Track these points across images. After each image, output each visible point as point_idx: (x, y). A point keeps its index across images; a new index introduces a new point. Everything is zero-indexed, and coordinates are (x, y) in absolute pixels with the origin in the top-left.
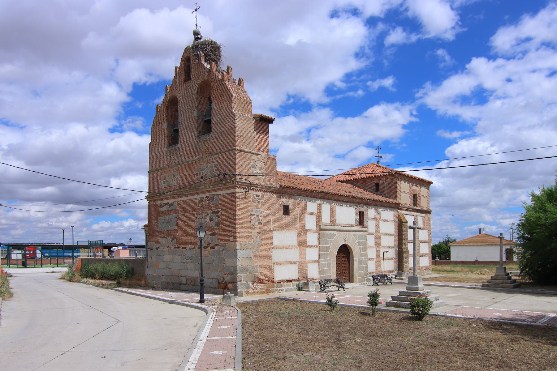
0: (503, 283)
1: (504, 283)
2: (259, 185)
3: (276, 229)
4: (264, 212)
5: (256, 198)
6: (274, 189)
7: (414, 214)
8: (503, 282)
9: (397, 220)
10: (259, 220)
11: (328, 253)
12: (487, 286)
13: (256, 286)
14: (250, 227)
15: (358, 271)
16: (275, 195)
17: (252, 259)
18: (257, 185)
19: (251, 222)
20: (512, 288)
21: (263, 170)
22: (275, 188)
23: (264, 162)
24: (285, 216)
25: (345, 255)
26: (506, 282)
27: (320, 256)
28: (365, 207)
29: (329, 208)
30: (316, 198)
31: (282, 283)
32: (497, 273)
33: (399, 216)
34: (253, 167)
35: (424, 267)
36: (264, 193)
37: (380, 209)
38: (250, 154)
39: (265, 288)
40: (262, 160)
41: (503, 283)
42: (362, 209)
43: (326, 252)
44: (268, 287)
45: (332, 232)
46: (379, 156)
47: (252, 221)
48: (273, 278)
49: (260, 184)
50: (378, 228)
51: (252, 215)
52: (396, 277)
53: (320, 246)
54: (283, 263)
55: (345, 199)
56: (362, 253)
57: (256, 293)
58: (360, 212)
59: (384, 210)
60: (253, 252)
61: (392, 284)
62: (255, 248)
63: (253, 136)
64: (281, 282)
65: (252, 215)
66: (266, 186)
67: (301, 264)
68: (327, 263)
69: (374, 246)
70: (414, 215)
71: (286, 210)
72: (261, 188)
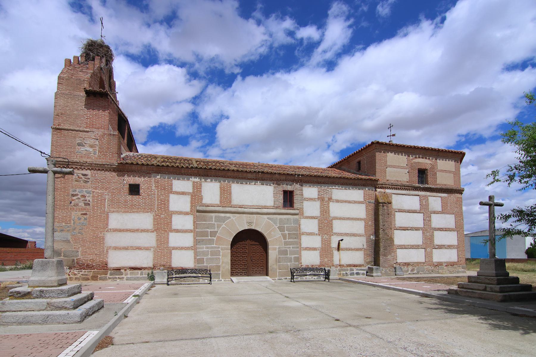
0: (485, 290)
1: (488, 289)
2: (85, 164)
3: (115, 210)
4: (94, 192)
5: (83, 177)
6: (109, 166)
7: (419, 194)
8: (486, 287)
9: (373, 201)
10: (86, 200)
11: (214, 239)
12: (454, 293)
13: (76, 272)
14: (69, 208)
15: (279, 262)
16: (114, 174)
17: (70, 242)
18: (81, 163)
19: (71, 203)
20: (498, 301)
21: (96, 147)
22: (112, 165)
23: (97, 139)
24: (131, 196)
25: (257, 243)
26: (491, 288)
27: (197, 242)
28: (298, 186)
29: (219, 186)
30: (191, 175)
31: (122, 271)
32: (481, 271)
33: (375, 196)
34: (79, 145)
35: (445, 262)
36: (95, 172)
37: (330, 187)
38: (74, 132)
39: (91, 274)
40: (94, 137)
41: (485, 290)
42: (289, 188)
43: (210, 238)
44: (95, 274)
45: (223, 215)
46: (391, 135)
47: (73, 202)
48: (106, 265)
49: (86, 162)
50: (325, 211)
51: (73, 195)
52: (367, 273)
53: (197, 230)
54: (126, 248)
55: (249, 176)
56: (287, 240)
57: (74, 279)
58: (285, 192)
59: (340, 188)
60: (73, 235)
61: (329, 281)
62: (77, 231)
63: (81, 113)
64: (120, 270)
65: (73, 195)
66: (95, 164)
67: (159, 251)
68: (211, 251)
69: (317, 233)
70: (418, 195)
71: (134, 190)
72: (90, 166)
